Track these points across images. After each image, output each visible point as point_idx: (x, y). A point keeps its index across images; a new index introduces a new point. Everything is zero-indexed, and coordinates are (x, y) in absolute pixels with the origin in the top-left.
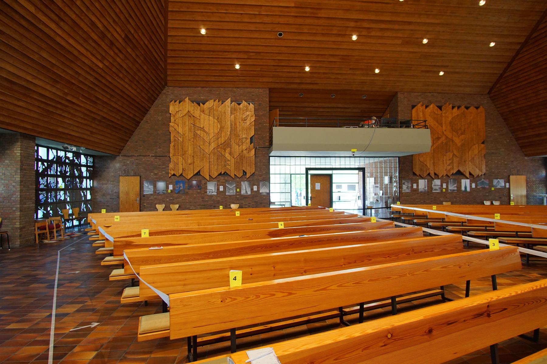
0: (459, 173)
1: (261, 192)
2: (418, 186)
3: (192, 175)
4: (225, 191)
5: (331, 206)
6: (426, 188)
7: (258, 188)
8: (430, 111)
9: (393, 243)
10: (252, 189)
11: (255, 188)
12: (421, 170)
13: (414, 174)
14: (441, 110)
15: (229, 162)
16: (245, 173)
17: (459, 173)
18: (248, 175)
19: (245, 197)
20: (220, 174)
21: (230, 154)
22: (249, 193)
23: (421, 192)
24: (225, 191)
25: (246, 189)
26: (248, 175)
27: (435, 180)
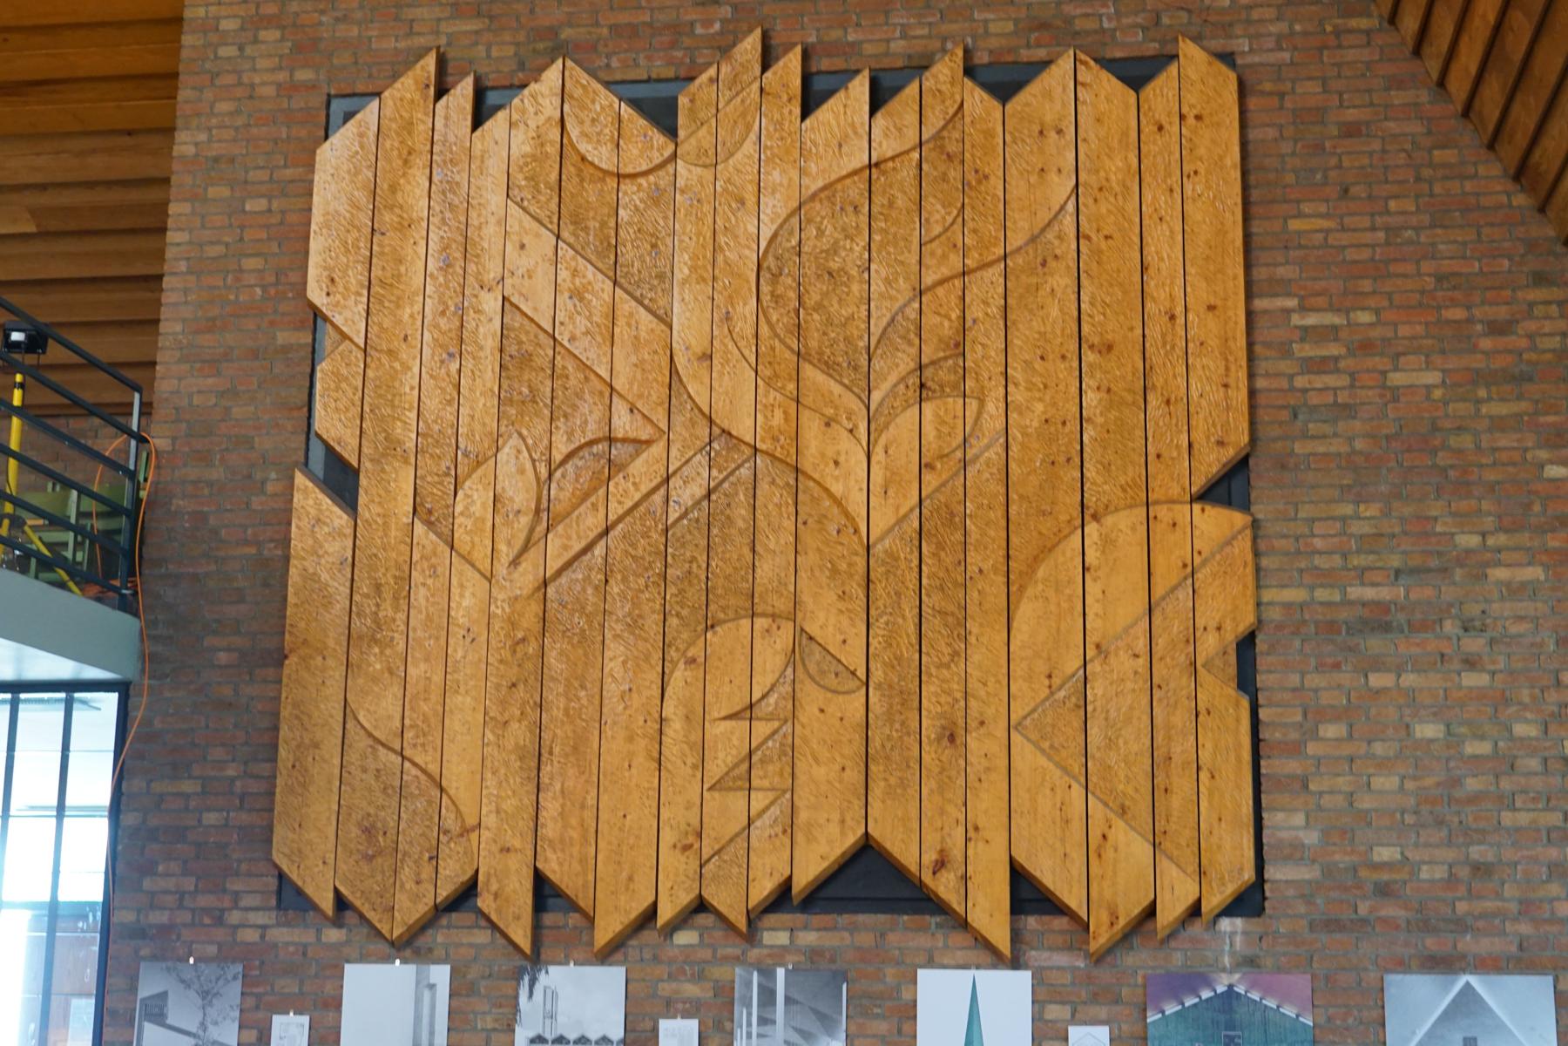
0: (869, 882)
3: (423, 907)
8: (522, 144)
12: (375, 842)
14: (671, 131)
17: (869, 882)
27: (555, 977)
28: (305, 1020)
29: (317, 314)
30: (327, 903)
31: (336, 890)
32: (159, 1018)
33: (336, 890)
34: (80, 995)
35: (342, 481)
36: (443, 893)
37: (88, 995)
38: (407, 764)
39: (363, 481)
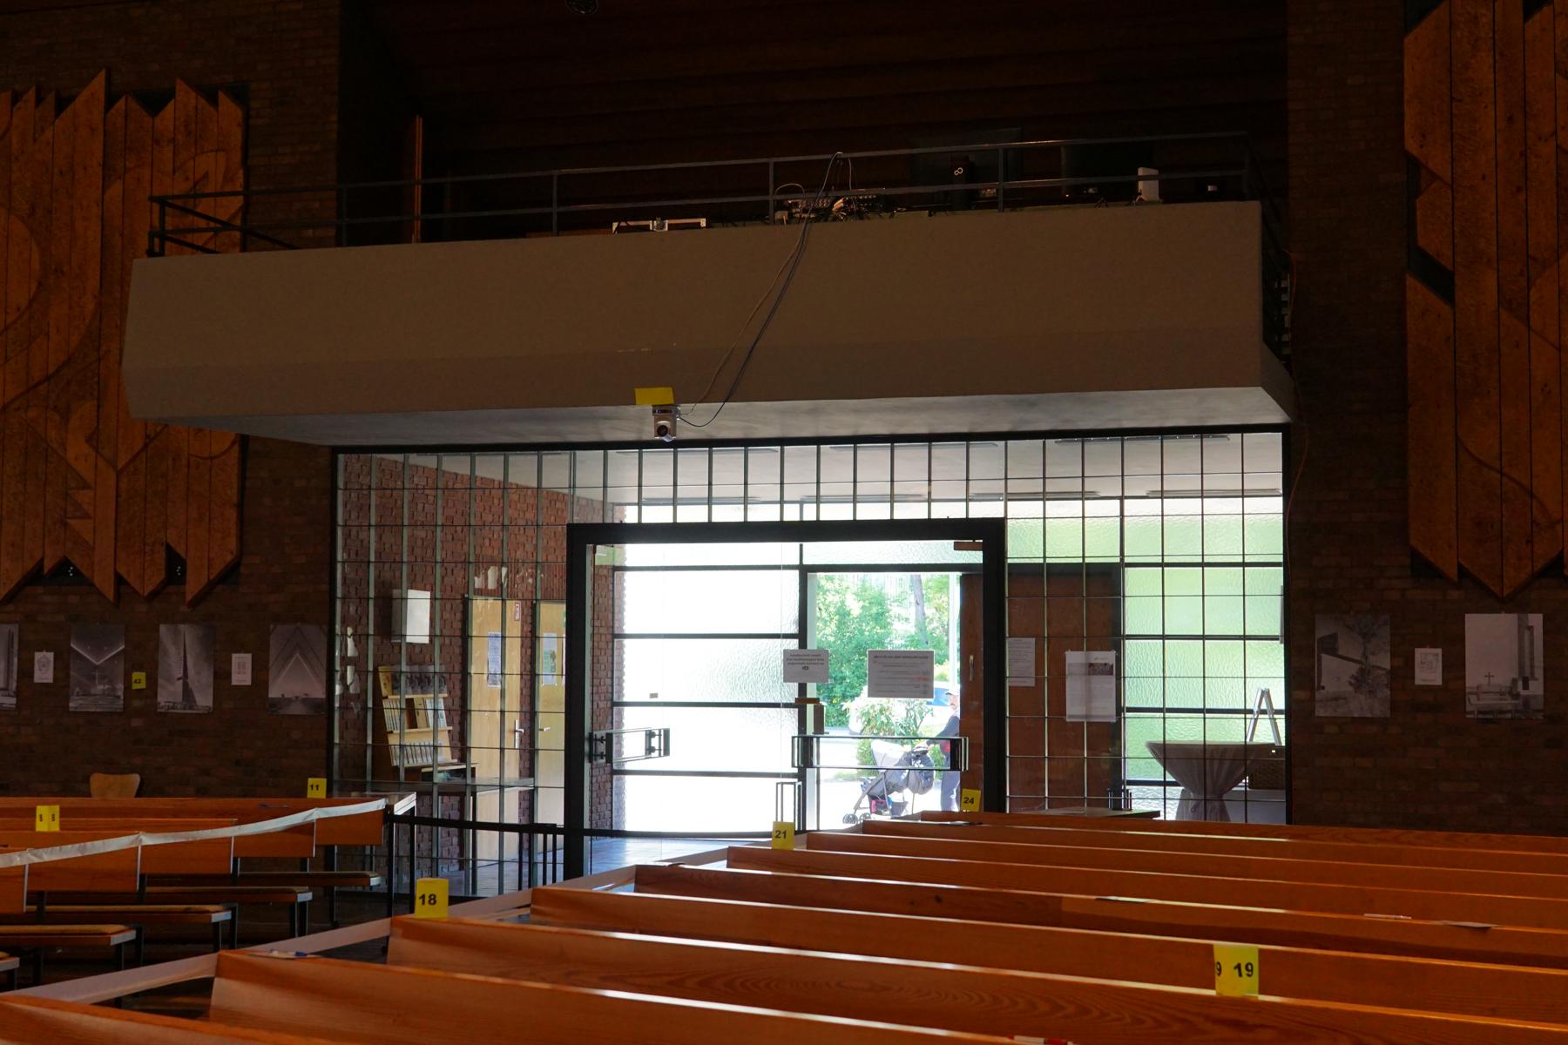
1: (274, 692)
2: (1454, 665)
4: (61, 686)
5: (412, 911)
6: (1537, 688)
7: (260, 670)
9: (1302, 1008)
10: (222, 675)
11: (241, 671)
13: (1423, 570)
15: (84, 497)
16: (175, 565)
18: (192, 587)
19: (182, 727)
20: (35, 577)
21: (93, 439)
22: (204, 700)
23: (1489, 718)
24: (61, 686)
25: (184, 674)
26: (192, 587)
28: (1439, 651)
29: (1414, 165)
30: (1453, 573)
31: (1460, 565)
32: (1333, 651)
33: (1460, 565)
34: (549, 598)
35: (1441, 280)
36: (1539, 566)
37: (558, 600)
38: (1505, 480)
39: (1458, 281)
